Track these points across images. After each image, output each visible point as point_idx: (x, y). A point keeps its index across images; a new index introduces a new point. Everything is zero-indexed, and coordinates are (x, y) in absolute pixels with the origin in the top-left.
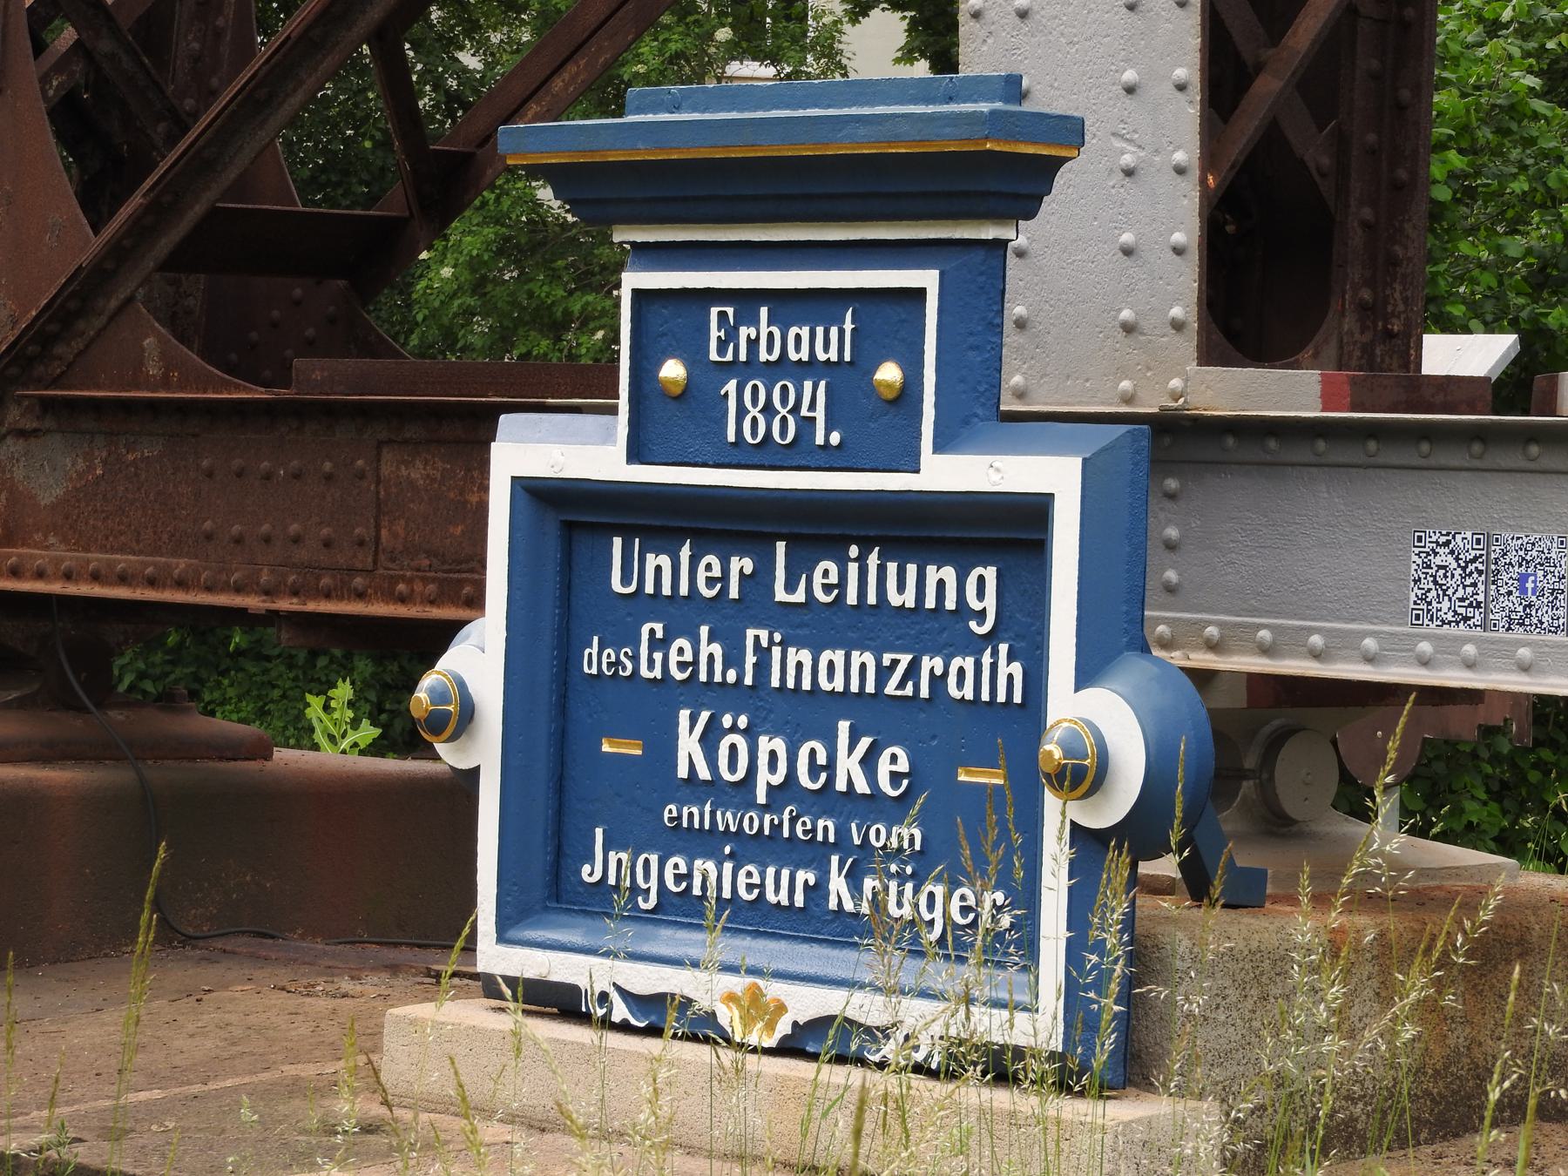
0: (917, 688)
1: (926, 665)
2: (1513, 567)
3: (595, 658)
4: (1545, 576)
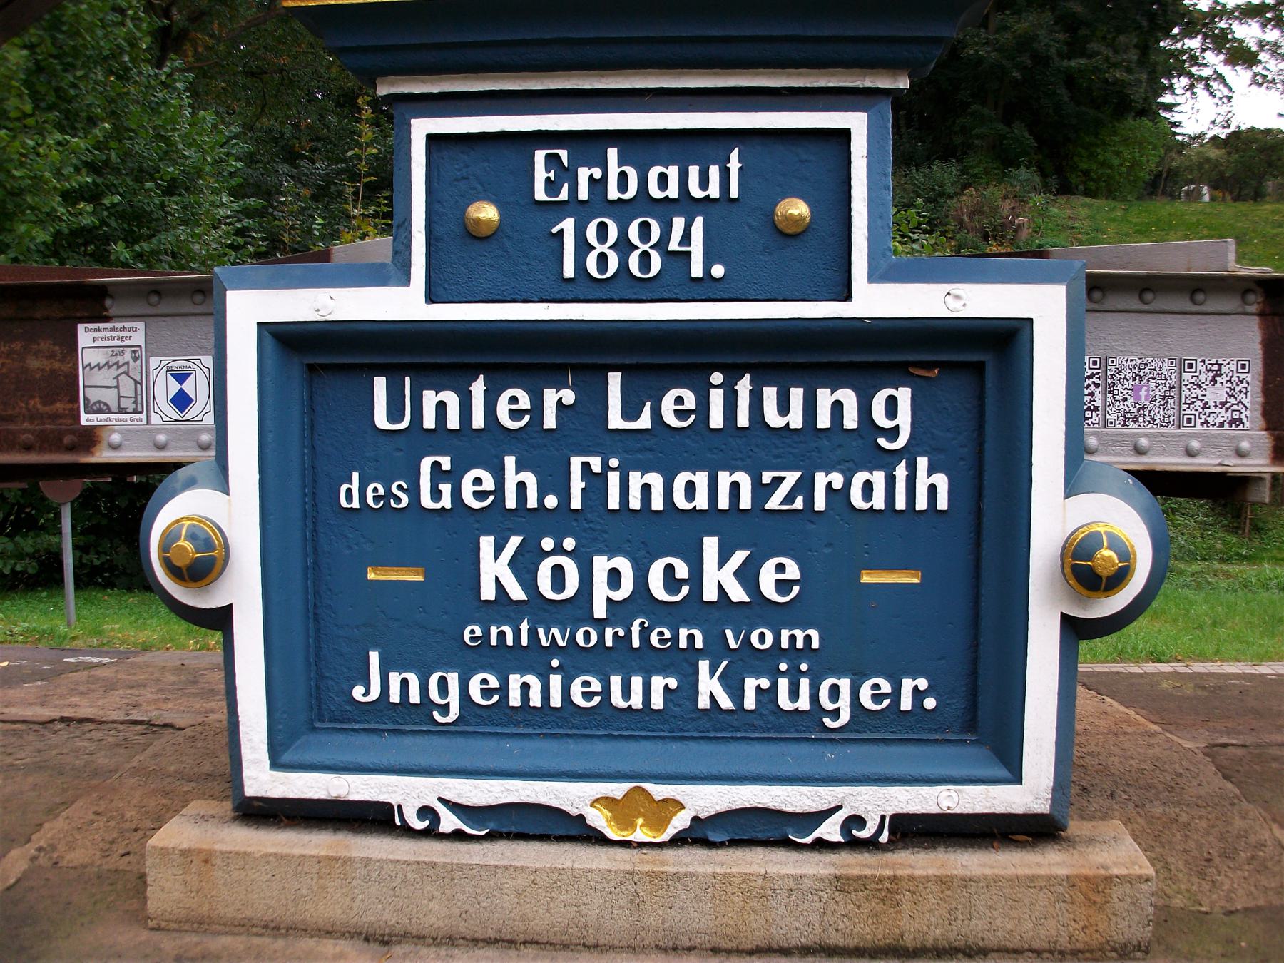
1: (821, 480)
2: (1127, 380)
4: (1157, 387)
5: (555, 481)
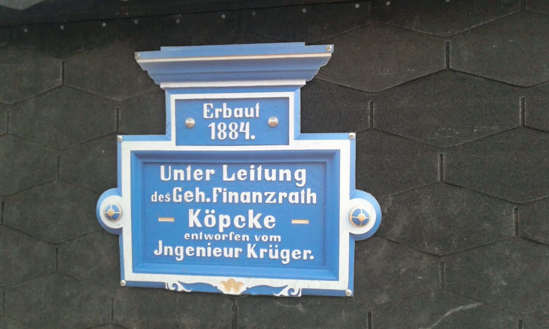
0: (277, 200)
3: (155, 197)
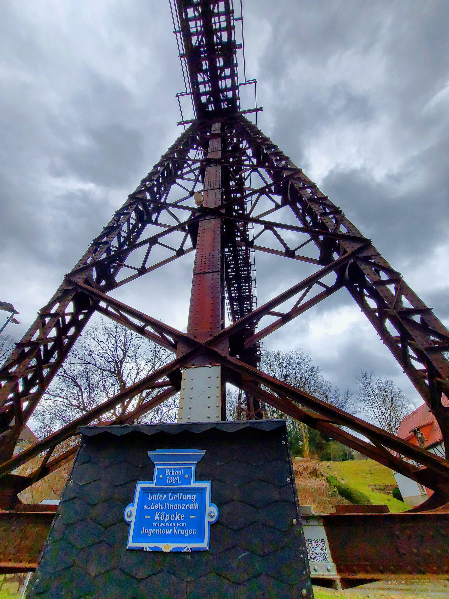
1: (187, 505)
5: (163, 506)
